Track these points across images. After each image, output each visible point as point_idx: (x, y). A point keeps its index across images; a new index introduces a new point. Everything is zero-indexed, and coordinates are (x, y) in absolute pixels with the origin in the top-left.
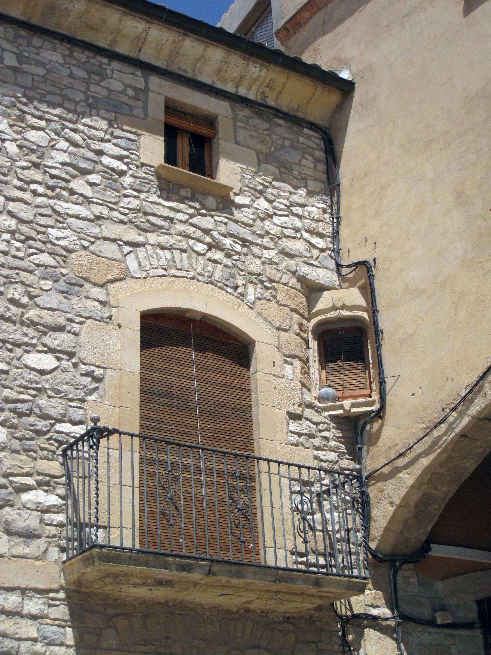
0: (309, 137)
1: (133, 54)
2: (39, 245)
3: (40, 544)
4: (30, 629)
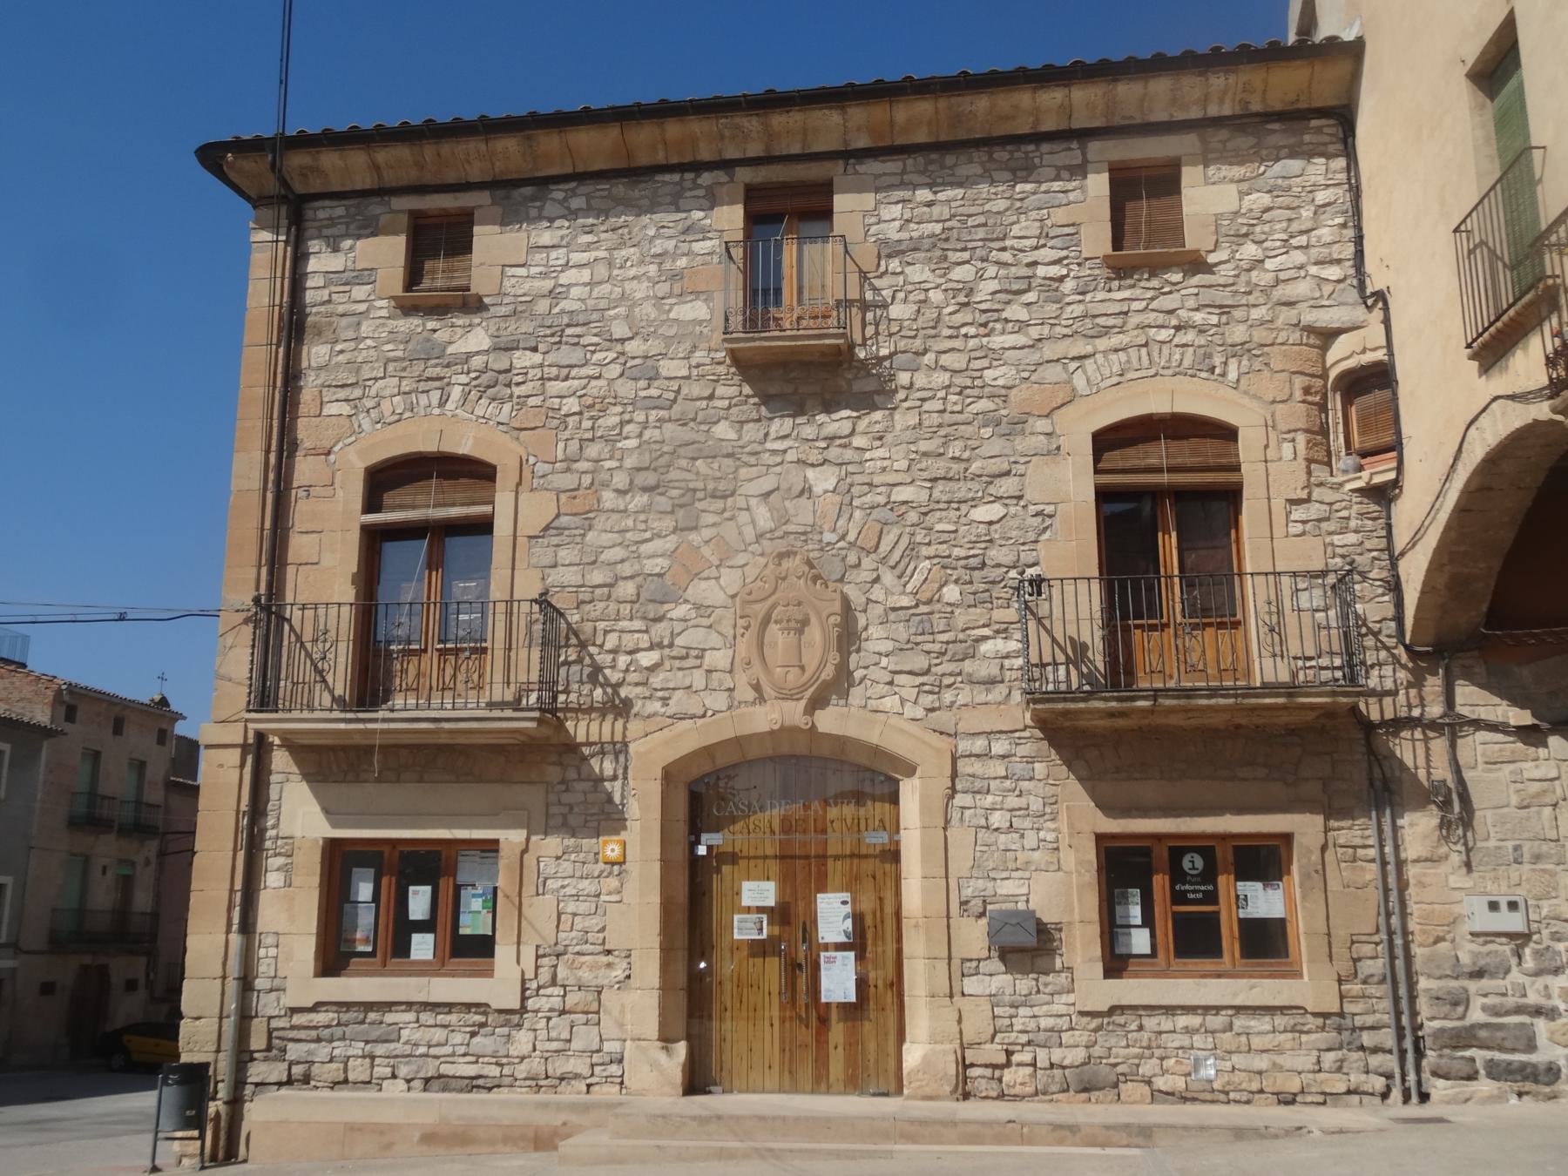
0: (1319, 130)
1: (1063, 126)
2: (976, 392)
3: (999, 692)
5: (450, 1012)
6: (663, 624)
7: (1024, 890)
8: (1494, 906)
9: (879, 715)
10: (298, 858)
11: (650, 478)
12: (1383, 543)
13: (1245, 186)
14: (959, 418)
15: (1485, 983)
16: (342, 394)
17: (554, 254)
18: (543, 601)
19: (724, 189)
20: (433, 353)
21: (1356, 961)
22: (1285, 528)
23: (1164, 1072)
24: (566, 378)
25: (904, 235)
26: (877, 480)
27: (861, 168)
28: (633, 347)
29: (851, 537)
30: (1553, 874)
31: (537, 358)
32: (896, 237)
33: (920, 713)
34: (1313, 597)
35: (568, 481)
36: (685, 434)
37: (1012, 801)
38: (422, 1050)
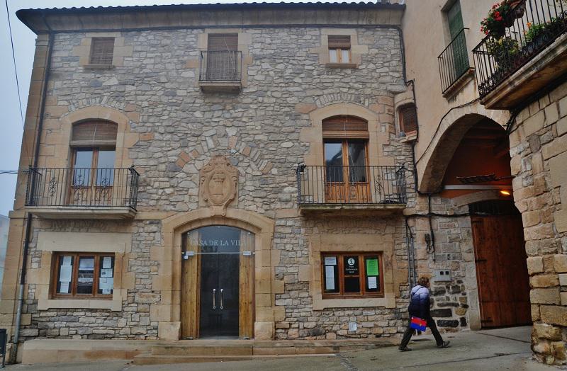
2: (284, 105)
3: (291, 204)
4: (289, 230)
5: (96, 312)
6: (175, 179)
7: (297, 271)
8: (442, 273)
9: (248, 210)
10: (43, 258)
11: (172, 129)
12: (411, 159)
13: (370, 46)
14: (279, 113)
15: (438, 297)
16: (65, 98)
17: (142, 53)
18: (132, 170)
19: (201, 35)
20: (97, 85)
21: (401, 291)
22: (379, 155)
23: (341, 329)
24: (144, 95)
25: (261, 53)
26: (250, 132)
27: (247, 31)
28: (167, 85)
29: (241, 151)
30: (458, 263)
31: (134, 88)
32: (259, 54)
33: (263, 211)
34: (391, 176)
35: (143, 129)
36: (184, 115)
37: (293, 241)
38: (87, 325)
